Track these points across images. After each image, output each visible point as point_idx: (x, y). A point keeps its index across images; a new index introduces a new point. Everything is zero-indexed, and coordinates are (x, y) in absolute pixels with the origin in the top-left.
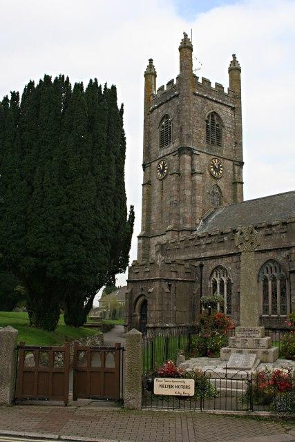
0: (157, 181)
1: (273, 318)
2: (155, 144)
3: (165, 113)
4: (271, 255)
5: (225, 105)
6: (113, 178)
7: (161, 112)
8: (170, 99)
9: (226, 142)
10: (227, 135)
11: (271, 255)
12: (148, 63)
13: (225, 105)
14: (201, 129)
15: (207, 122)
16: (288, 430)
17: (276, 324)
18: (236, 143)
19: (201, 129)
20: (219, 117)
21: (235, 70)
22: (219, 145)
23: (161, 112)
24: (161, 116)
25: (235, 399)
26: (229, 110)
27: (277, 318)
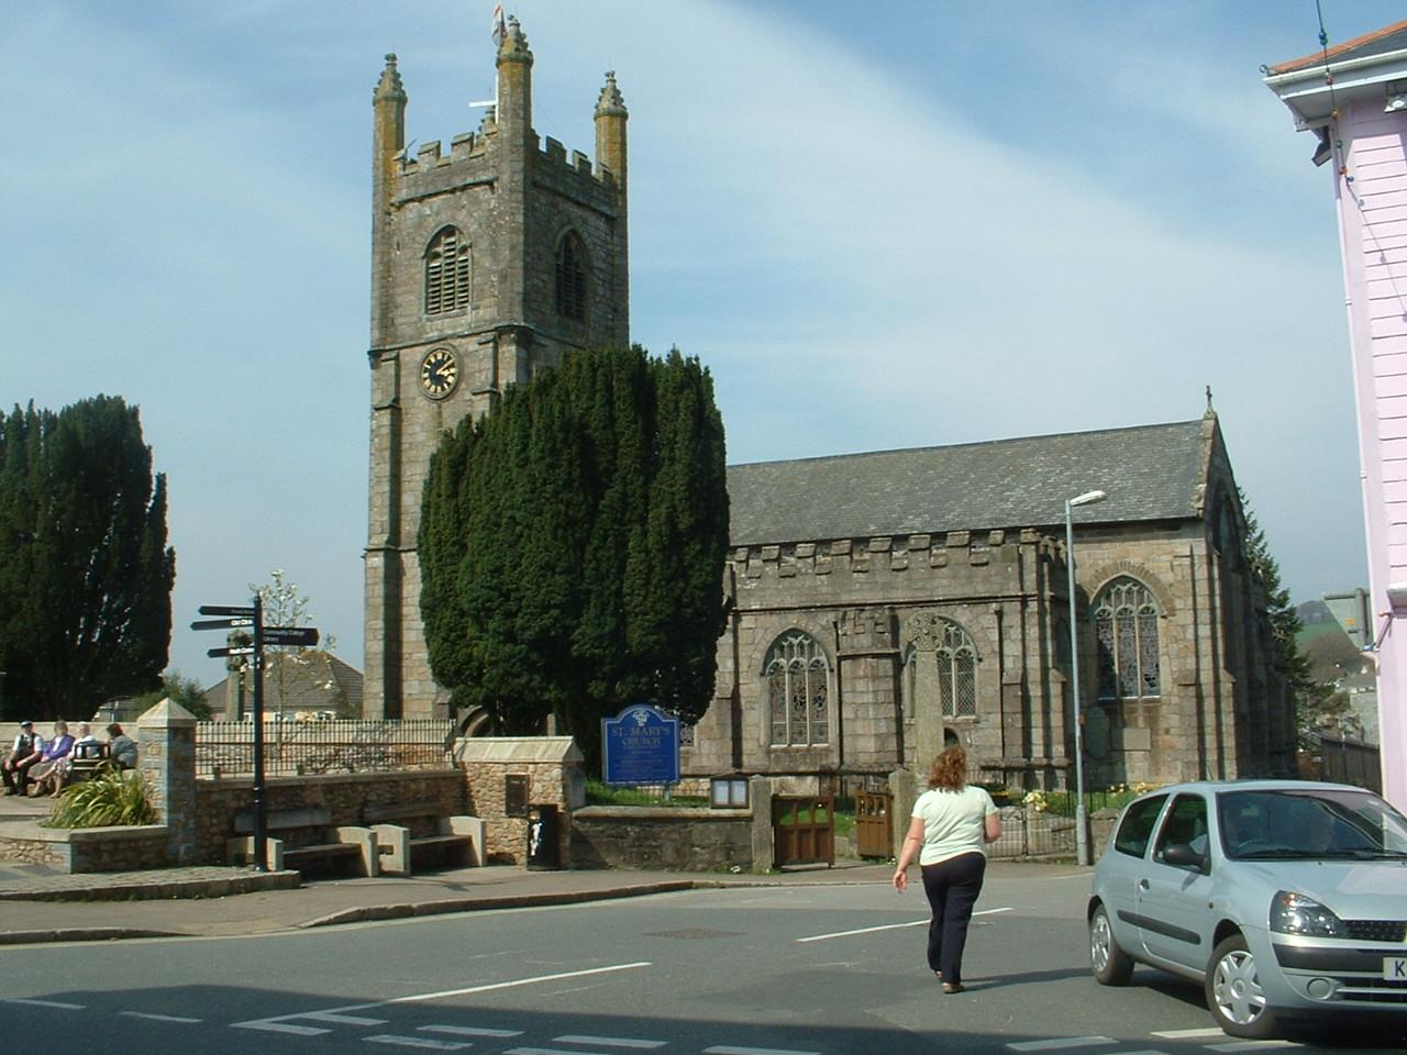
0: (421, 402)
1: (798, 750)
2: (411, 302)
3: (446, 219)
4: (793, 620)
5: (594, 210)
6: (1226, 813)
7: (435, 213)
8: (465, 188)
9: (595, 312)
10: (597, 288)
11: (793, 620)
12: (383, 66)
13: (594, 210)
14: (545, 277)
15: (557, 256)
16: (330, 760)
17: (805, 763)
18: (615, 310)
19: (545, 277)
20: (579, 238)
21: (615, 116)
22: (580, 316)
23: (435, 213)
24: (432, 227)
25: (243, 731)
26: (601, 224)
27: (808, 750)
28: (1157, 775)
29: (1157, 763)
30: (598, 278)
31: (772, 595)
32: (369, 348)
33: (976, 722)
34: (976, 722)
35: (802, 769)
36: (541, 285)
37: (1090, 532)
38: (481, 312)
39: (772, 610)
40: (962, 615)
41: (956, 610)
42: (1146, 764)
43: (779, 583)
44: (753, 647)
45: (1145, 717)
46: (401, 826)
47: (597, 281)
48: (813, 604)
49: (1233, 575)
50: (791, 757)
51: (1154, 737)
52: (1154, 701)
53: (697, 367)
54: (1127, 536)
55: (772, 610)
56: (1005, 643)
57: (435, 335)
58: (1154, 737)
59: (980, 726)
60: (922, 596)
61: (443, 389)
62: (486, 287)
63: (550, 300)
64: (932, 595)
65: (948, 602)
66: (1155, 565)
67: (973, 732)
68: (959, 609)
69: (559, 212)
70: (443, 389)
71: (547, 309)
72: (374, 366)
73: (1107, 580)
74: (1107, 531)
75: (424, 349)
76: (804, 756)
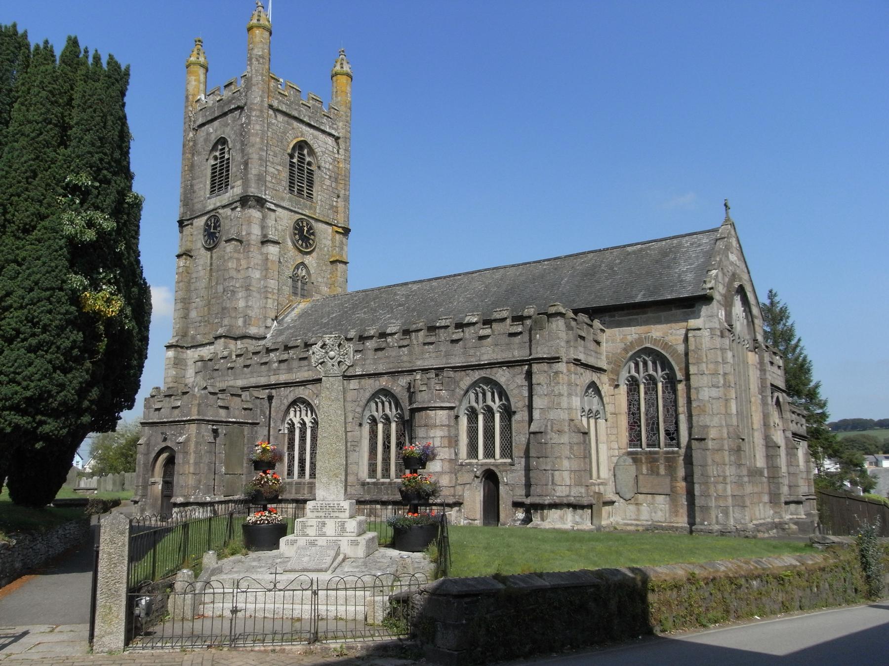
3: (220, 134)
4: (384, 382)
7: (213, 131)
17: (388, 494)
19: (280, 168)
24: (213, 139)
26: (330, 141)
28: (676, 516)
29: (676, 506)
30: (326, 174)
31: (370, 364)
32: (178, 219)
33: (512, 465)
34: (512, 465)
35: (385, 498)
36: (276, 172)
37: (620, 312)
38: (235, 189)
39: (370, 376)
40: (502, 376)
41: (498, 371)
42: (667, 506)
43: (375, 355)
44: (357, 403)
45: (665, 466)
46: (555, 530)
47: (325, 176)
48: (397, 370)
49: (750, 354)
50: (378, 488)
51: (674, 484)
52: (673, 452)
53: (15, 33)
54: (650, 315)
55: (370, 376)
56: (535, 398)
57: (211, 207)
58: (674, 484)
59: (513, 468)
60: (473, 361)
61: (214, 241)
62: (238, 173)
63: (284, 183)
64: (480, 360)
65: (491, 365)
66: (674, 337)
67: (509, 472)
68: (500, 370)
69: (293, 128)
70: (214, 241)
71: (281, 188)
72: (181, 232)
73: (633, 352)
74: (635, 311)
75: (206, 218)
76: (387, 489)
